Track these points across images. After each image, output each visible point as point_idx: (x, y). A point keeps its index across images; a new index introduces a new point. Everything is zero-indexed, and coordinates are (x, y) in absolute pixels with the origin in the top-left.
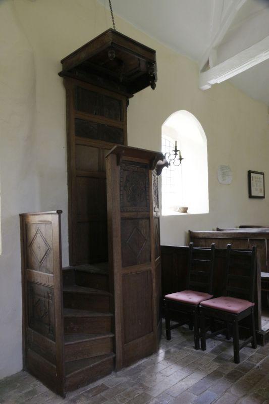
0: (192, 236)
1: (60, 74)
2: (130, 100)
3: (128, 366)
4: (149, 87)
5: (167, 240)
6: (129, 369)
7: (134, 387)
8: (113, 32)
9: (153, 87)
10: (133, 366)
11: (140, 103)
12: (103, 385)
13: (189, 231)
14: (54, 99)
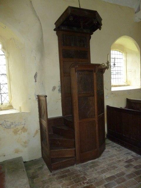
0: (128, 101)
1: (55, 30)
2: (91, 36)
3: (82, 163)
4: (98, 30)
5: (108, 102)
6: (83, 164)
7: (81, 173)
8: (70, 8)
9: (100, 30)
10: (85, 163)
11: (96, 39)
12: (69, 170)
13: (127, 98)
14: (53, 42)
